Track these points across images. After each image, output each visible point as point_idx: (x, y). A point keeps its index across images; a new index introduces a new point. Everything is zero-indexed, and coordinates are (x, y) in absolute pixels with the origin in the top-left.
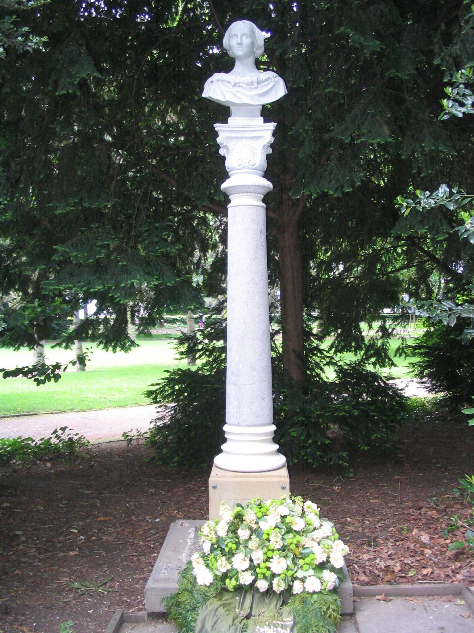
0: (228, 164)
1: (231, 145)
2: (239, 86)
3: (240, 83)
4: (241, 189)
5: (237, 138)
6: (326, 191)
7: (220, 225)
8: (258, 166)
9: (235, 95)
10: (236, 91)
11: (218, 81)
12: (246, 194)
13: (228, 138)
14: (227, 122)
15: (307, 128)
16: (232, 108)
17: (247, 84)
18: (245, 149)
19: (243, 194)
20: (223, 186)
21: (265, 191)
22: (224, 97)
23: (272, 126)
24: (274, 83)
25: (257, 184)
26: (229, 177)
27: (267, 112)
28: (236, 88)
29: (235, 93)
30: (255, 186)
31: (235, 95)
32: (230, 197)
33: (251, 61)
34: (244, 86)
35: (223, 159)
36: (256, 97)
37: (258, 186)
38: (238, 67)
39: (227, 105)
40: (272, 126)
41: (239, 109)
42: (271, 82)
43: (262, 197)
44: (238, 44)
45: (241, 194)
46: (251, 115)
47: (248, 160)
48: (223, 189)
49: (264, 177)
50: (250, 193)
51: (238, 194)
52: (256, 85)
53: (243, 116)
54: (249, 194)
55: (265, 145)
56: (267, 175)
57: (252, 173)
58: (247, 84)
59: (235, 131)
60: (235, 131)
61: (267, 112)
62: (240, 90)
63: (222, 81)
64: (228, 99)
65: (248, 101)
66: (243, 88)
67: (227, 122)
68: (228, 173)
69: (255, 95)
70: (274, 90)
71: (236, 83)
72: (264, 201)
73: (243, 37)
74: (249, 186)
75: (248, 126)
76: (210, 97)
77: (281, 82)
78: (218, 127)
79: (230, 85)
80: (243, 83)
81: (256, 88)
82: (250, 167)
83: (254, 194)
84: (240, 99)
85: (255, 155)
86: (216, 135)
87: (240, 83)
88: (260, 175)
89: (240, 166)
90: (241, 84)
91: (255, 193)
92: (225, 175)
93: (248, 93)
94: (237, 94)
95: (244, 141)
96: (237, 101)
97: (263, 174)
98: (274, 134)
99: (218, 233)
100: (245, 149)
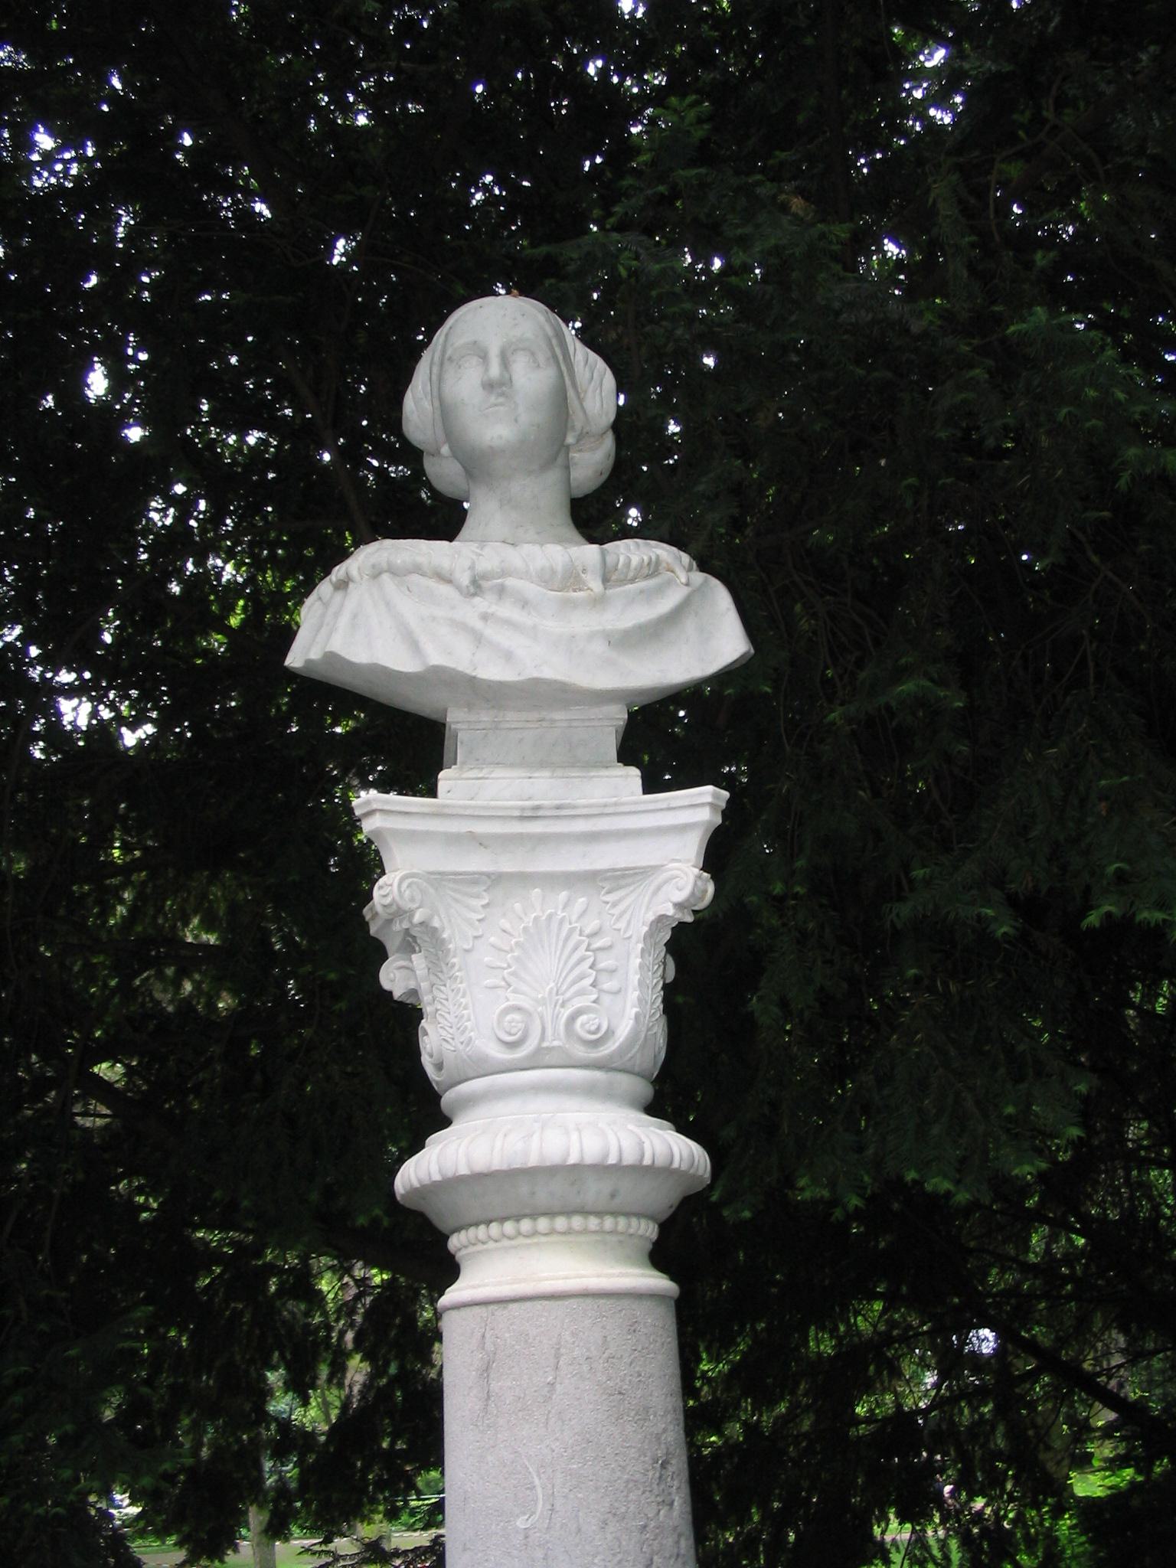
0: (436, 1041)
1: (458, 921)
2: (501, 591)
3: (504, 573)
4: (531, 1196)
5: (495, 880)
6: (911, 1175)
7: (358, 1297)
8: (611, 1056)
9: (478, 639)
10: (485, 617)
11: (376, 574)
12: (561, 1223)
13: (439, 879)
14: (432, 792)
15: (778, 888)
16: (457, 719)
17: (546, 579)
18: (538, 947)
19: (543, 1223)
20: (415, 1173)
21: (664, 1198)
22: (415, 646)
23: (699, 806)
24: (686, 591)
25: (629, 1159)
26: (444, 1122)
27: (662, 739)
28: (481, 604)
29: (479, 625)
30: (619, 1169)
31: (478, 639)
32: (454, 1242)
33: (545, 494)
34: (531, 590)
35: (406, 1018)
36: (599, 647)
37: (619, 1170)
38: (485, 512)
39: (422, 703)
40: (699, 806)
41: (496, 727)
42: (669, 583)
43: (649, 1230)
44: (489, 386)
45: (526, 1225)
46: (570, 759)
47: (566, 1013)
48: (415, 1192)
49: (654, 1109)
50: (584, 1212)
51: (509, 1227)
52: (596, 585)
53: (523, 763)
54: (577, 1222)
55: (662, 918)
56: (669, 1097)
57: (590, 1091)
58: (546, 579)
59: (480, 842)
60: (480, 842)
61: (662, 739)
62: (506, 610)
63: (393, 571)
64: (436, 659)
65: (554, 668)
66: (525, 604)
67: (432, 792)
68: (437, 1097)
69: (592, 636)
70: (690, 624)
71: (485, 577)
72: (660, 1257)
73: (501, 372)
74: (575, 1172)
75: (560, 812)
76: (331, 657)
77: (722, 599)
78: (378, 811)
79: (444, 589)
80: (525, 575)
81: (598, 602)
82: (581, 1052)
83: (609, 1222)
84: (508, 656)
85: (608, 985)
86: (366, 865)
87: (504, 573)
88: (633, 1104)
89: (512, 1045)
90: (510, 582)
91: (615, 1214)
92: (424, 1113)
93: (552, 625)
94: (489, 631)
95: (538, 904)
96: (492, 671)
97: (646, 1091)
98: (718, 855)
99: (351, 1325)
100: (538, 947)
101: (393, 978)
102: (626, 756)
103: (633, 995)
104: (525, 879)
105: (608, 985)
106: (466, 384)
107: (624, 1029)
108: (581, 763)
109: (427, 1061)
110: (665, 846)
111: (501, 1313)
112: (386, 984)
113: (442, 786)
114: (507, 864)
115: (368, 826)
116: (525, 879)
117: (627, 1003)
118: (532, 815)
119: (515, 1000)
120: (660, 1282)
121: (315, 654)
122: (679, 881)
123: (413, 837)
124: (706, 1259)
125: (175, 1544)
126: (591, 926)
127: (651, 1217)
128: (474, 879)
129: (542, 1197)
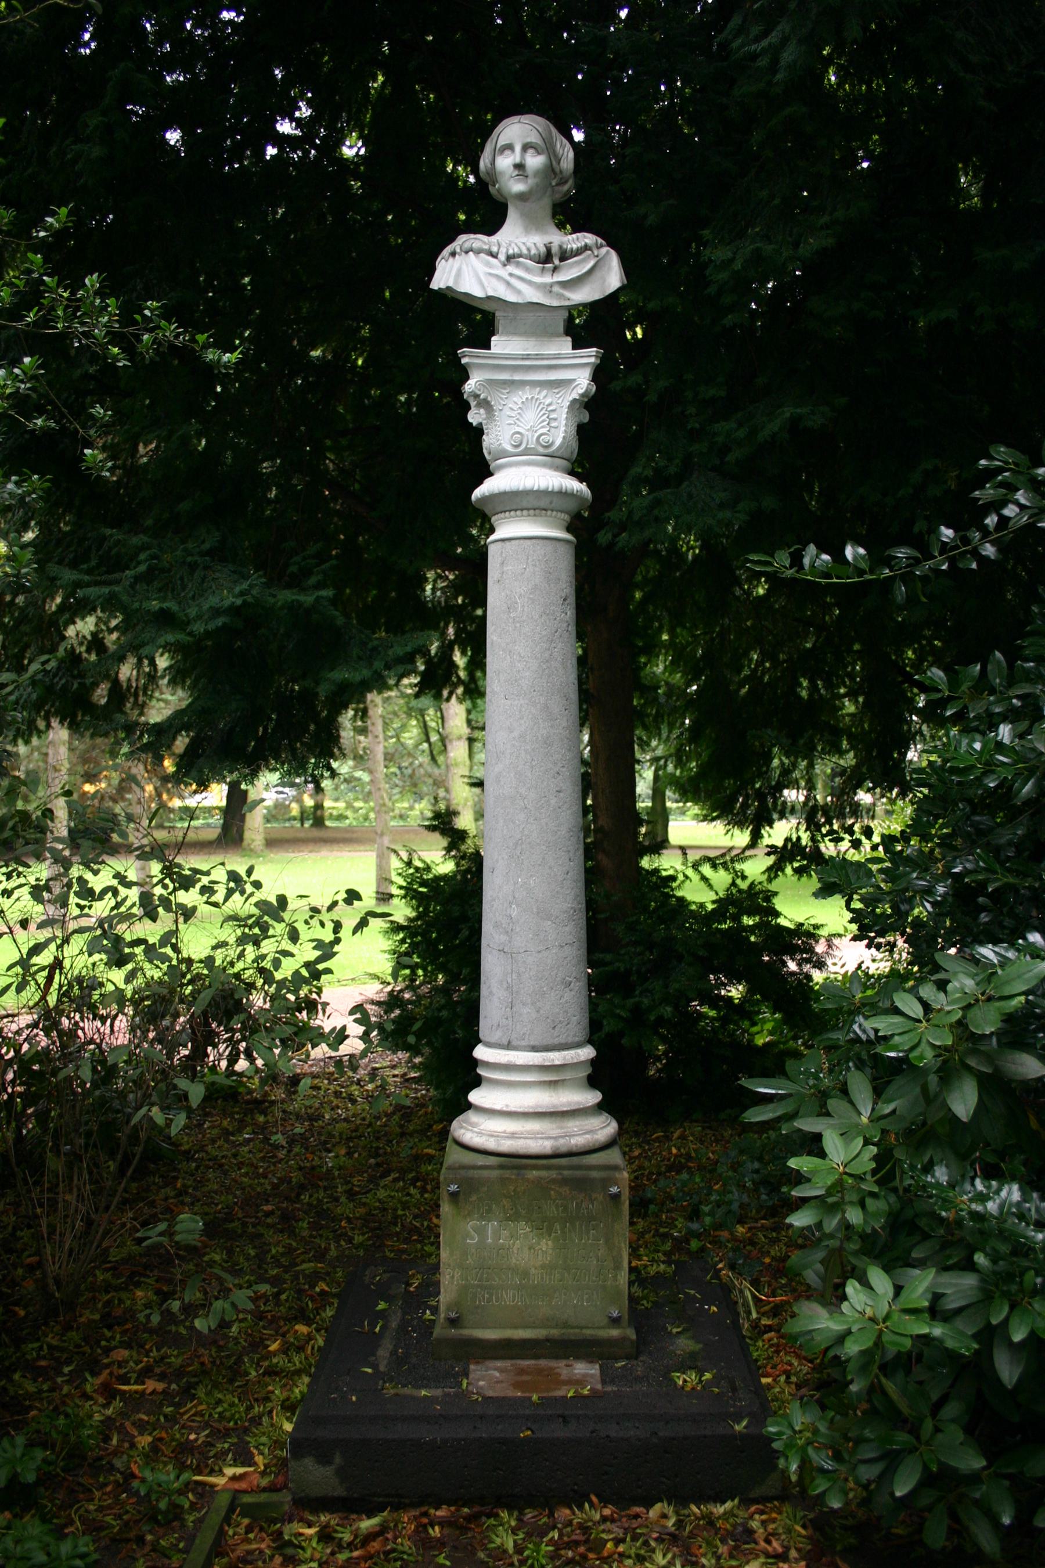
0: (488, 442)
5: (512, 383)
13: (491, 382)
18: (528, 415)
21: (572, 505)
23: (590, 356)
26: (490, 474)
28: (510, 268)
29: (508, 278)
40: (590, 356)
43: (567, 517)
48: (478, 500)
49: (572, 473)
57: (544, 465)
61: (588, 326)
64: (491, 293)
72: (569, 529)
75: (538, 357)
77: (614, 261)
82: (541, 450)
84: (519, 292)
92: (485, 472)
95: (526, 394)
96: (512, 298)
98: (598, 375)
100: (528, 415)
101: (474, 417)
102: (567, 333)
103: (563, 429)
104: (523, 383)
105: (554, 424)
106: (505, 163)
107: (558, 442)
108: (552, 335)
109: (485, 452)
110: (578, 371)
111: (508, 543)
112: (470, 420)
113: (492, 343)
114: (517, 377)
115: (464, 361)
116: (523, 383)
117: (561, 432)
118: (527, 357)
119: (518, 429)
120: (568, 536)
121: (442, 286)
122: (582, 382)
123: (480, 366)
124: (585, 527)
125: (312, 825)
126: (548, 401)
127: (567, 513)
128: (505, 383)
129: (525, 504)
